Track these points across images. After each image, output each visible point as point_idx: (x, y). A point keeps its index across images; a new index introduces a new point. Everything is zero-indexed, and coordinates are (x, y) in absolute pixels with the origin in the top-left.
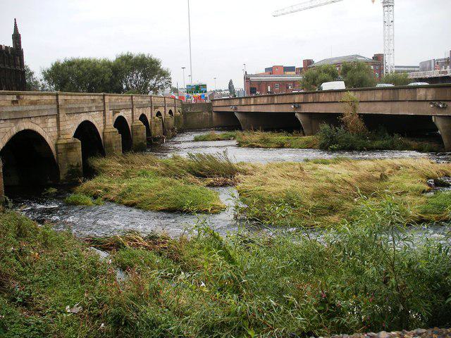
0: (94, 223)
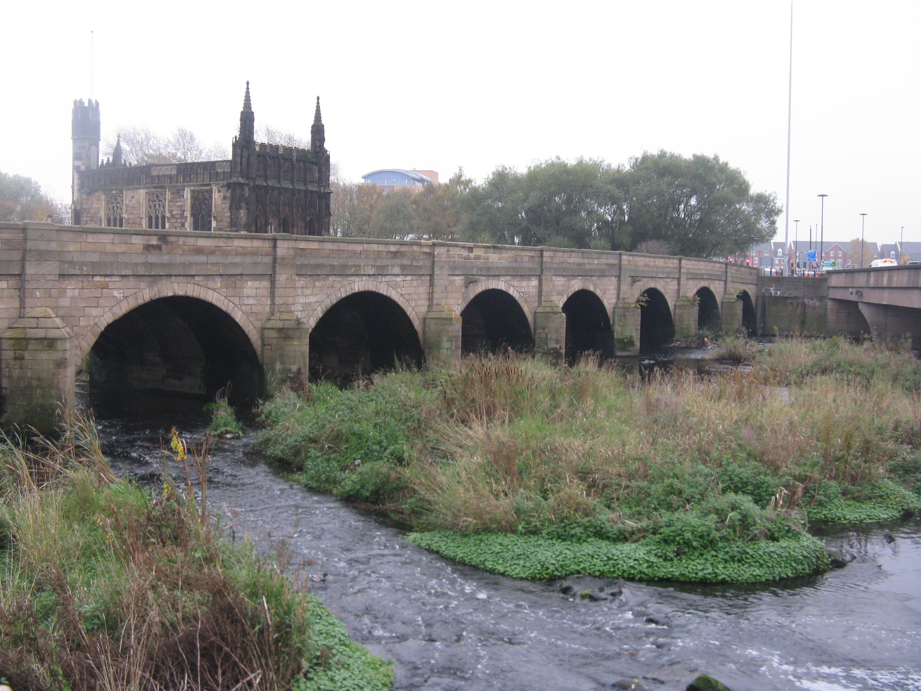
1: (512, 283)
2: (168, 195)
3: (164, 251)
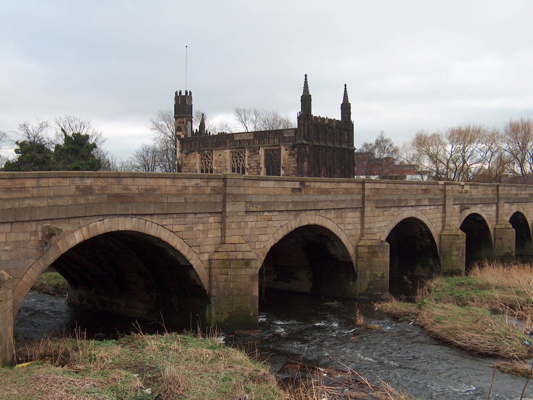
0: (481, 336)
1: (483, 209)
2: (247, 153)
3: (303, 193)
